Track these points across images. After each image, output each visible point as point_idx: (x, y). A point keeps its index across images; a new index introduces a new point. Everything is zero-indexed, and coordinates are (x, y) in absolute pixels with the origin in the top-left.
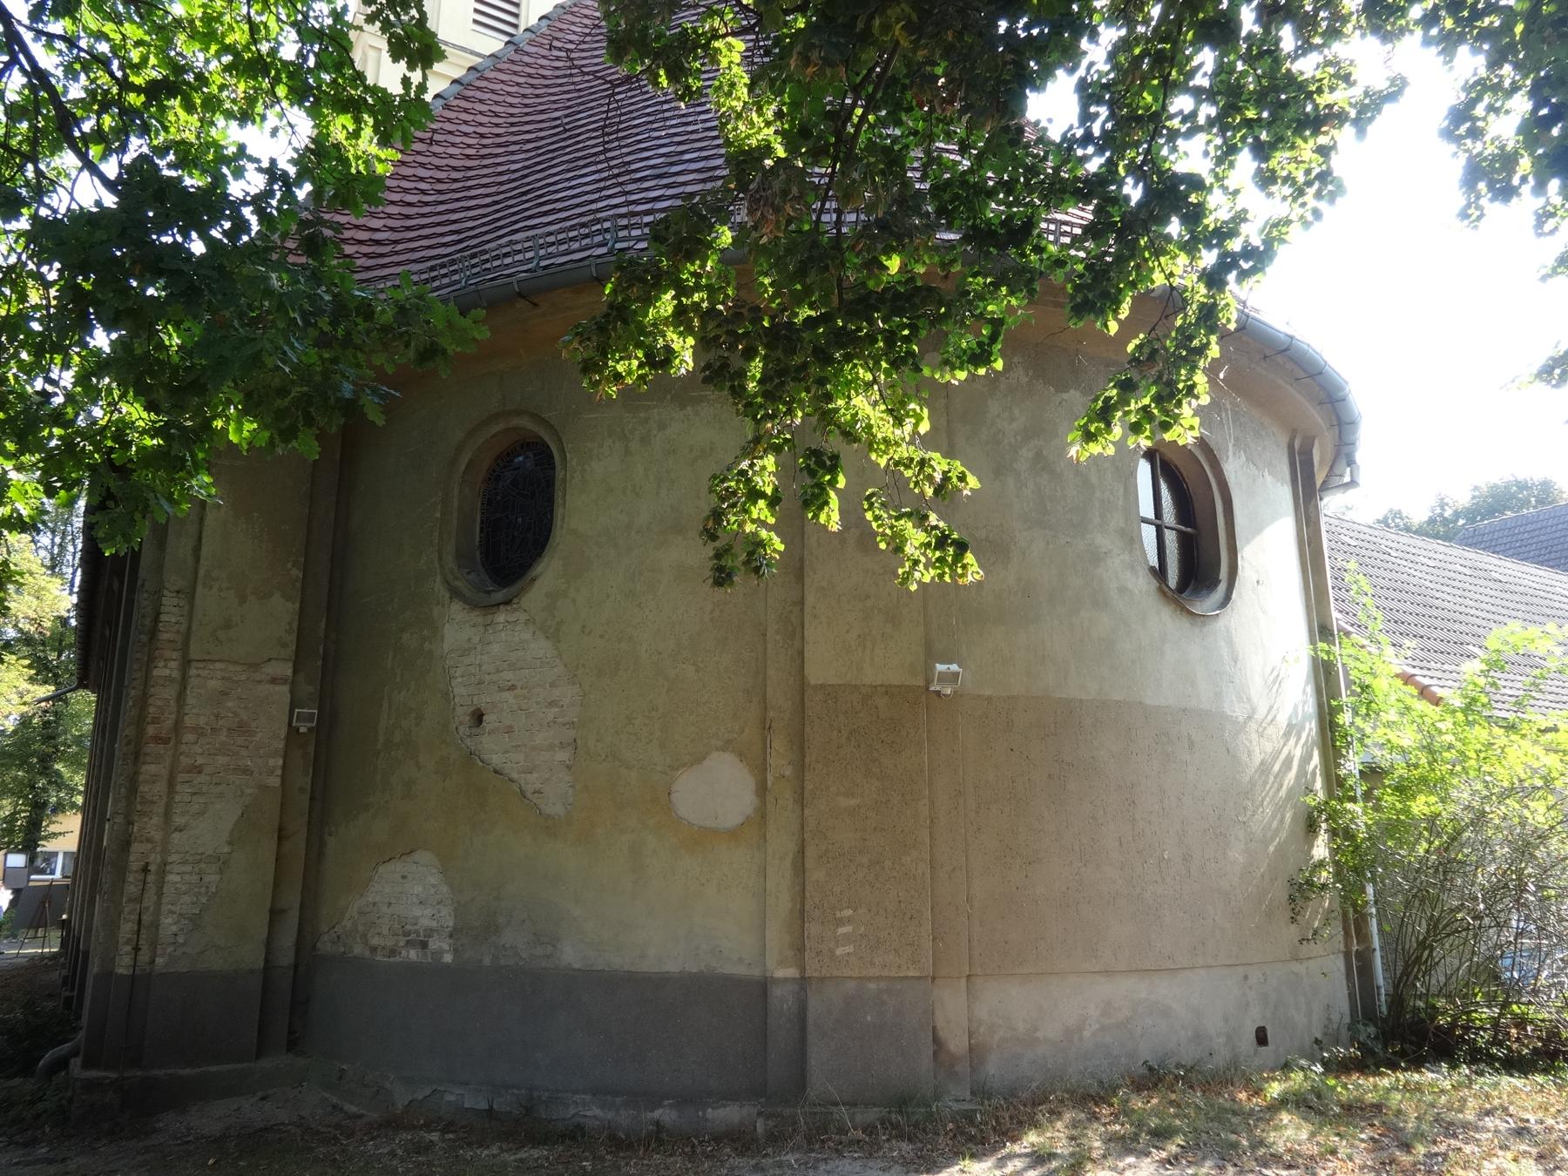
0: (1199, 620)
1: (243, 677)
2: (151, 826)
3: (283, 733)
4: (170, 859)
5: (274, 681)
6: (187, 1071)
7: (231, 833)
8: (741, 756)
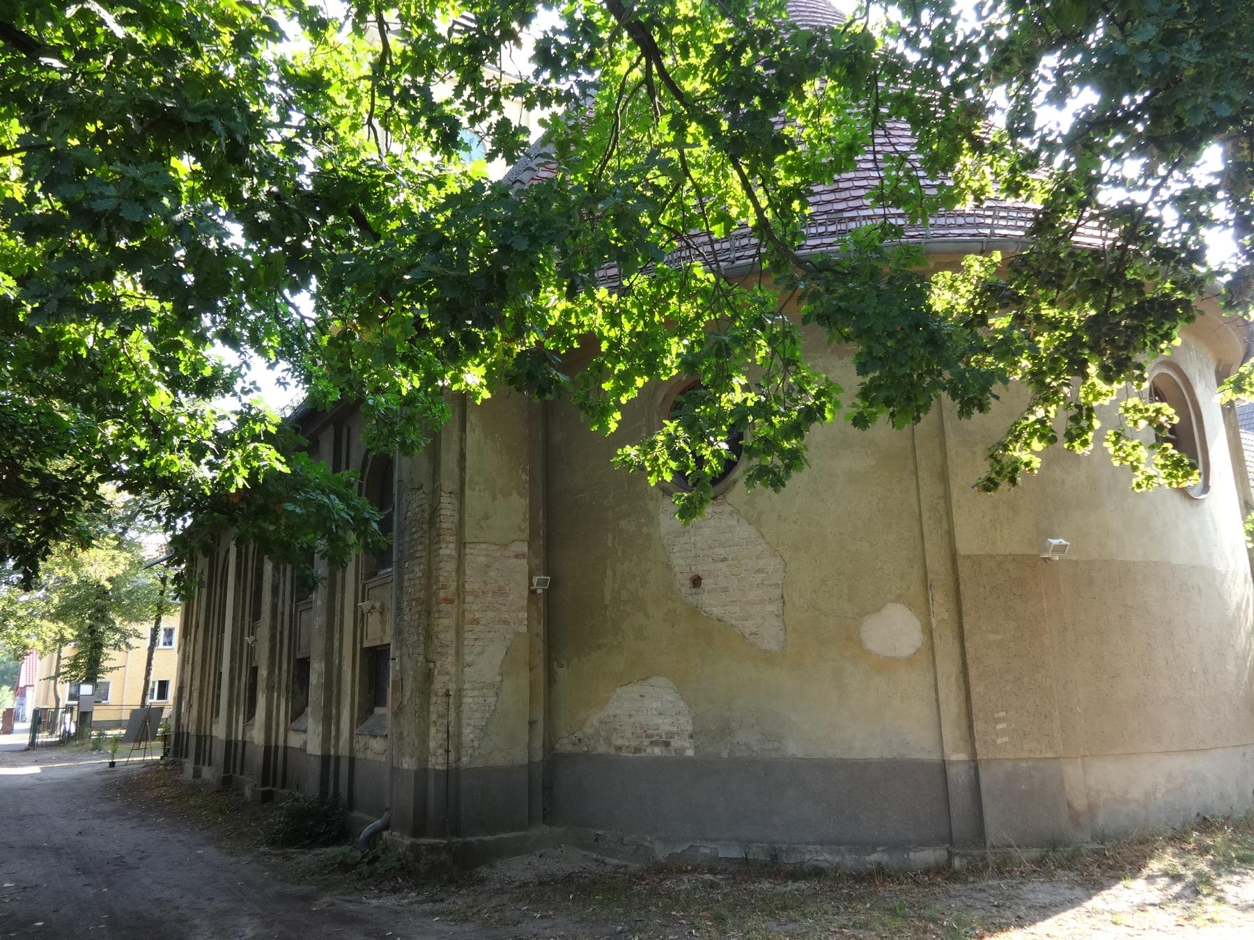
0: (1195, 502)
1: (499, 554)
2: (447, 663)
3: (526, 593)
4: (465, 687)
5: (517, 556)
6: (488, 838)
7: (501, 666)
8: (910, 606)
